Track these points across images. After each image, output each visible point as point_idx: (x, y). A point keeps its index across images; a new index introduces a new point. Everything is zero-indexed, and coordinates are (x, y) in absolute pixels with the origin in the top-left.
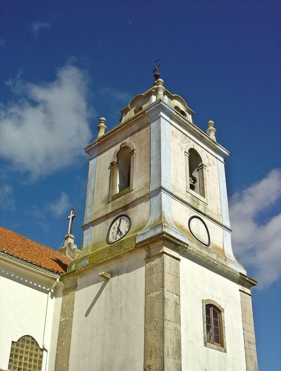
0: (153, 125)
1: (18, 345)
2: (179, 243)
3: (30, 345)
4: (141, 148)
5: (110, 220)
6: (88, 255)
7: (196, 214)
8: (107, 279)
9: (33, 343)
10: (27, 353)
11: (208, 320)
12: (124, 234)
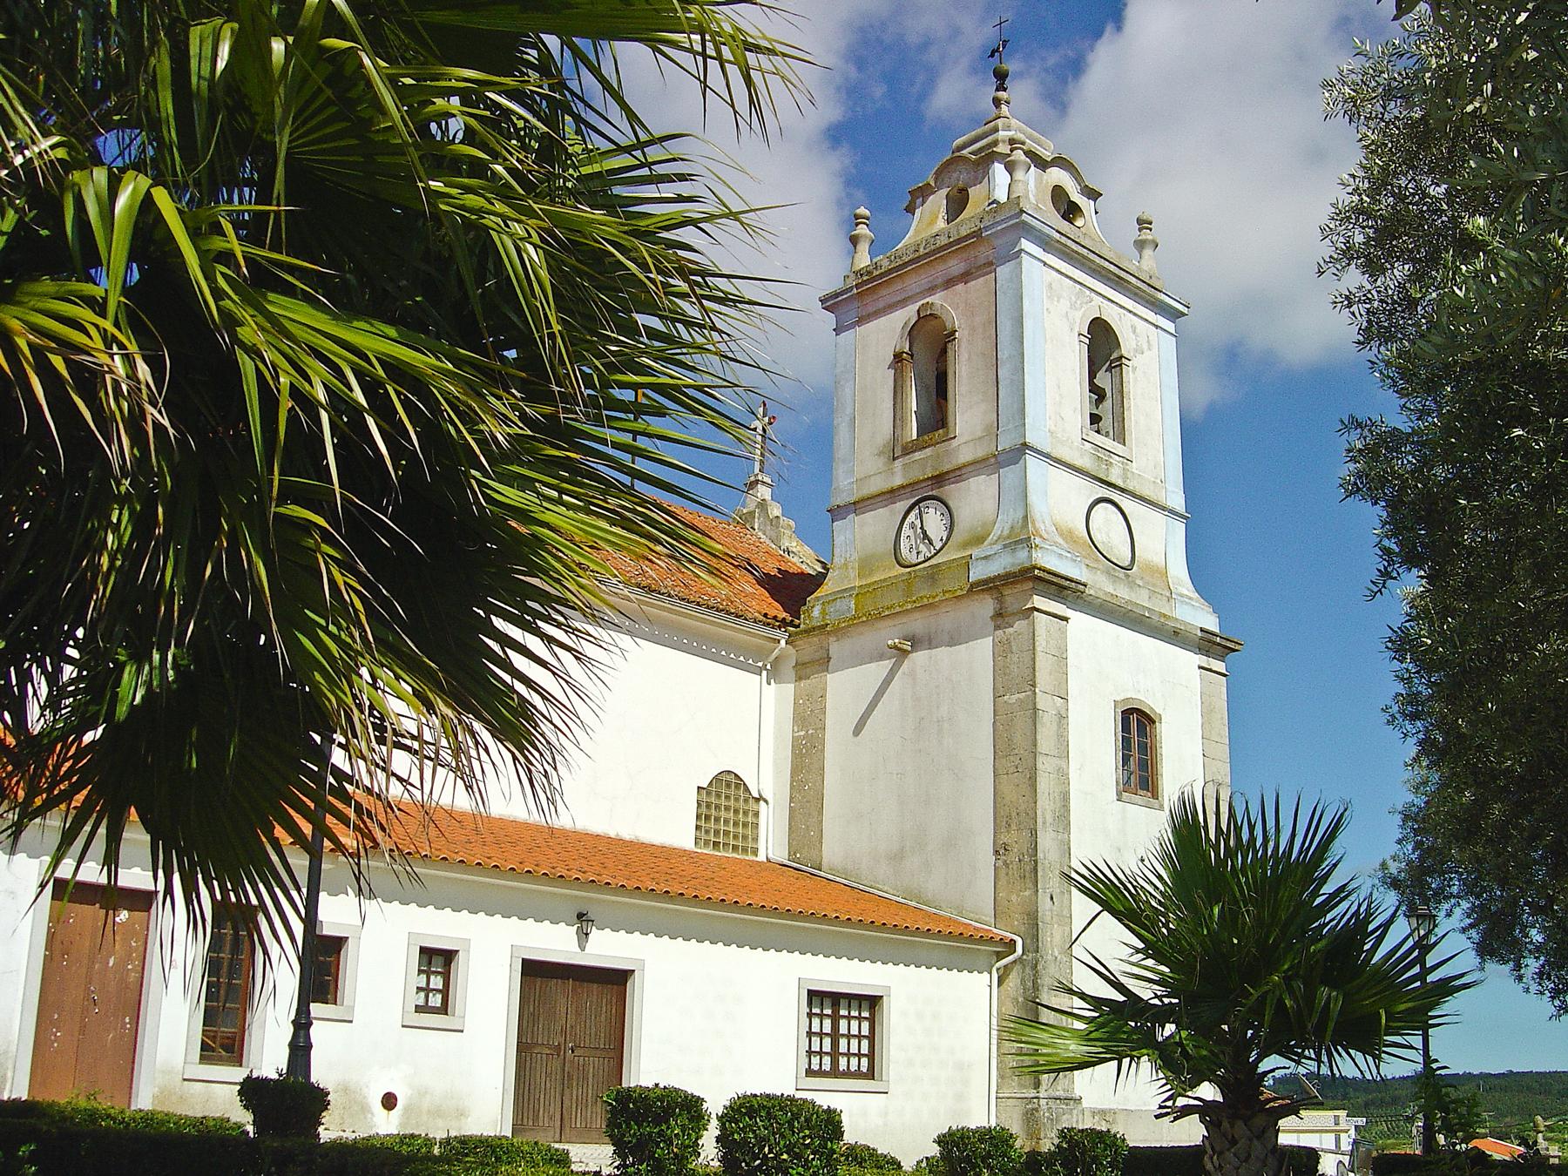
0: (1003, 271)
1: (709, 793)
2: (1067, 583)
3: (732, 791)
4: (973, 329)
5: (902, 506)
6: (853, 588)
7: (1105, 492)
8: (905, 653)
9: (737, 786)
10: (727, 808)
11: (1126, 744)
12: (938, 545)
